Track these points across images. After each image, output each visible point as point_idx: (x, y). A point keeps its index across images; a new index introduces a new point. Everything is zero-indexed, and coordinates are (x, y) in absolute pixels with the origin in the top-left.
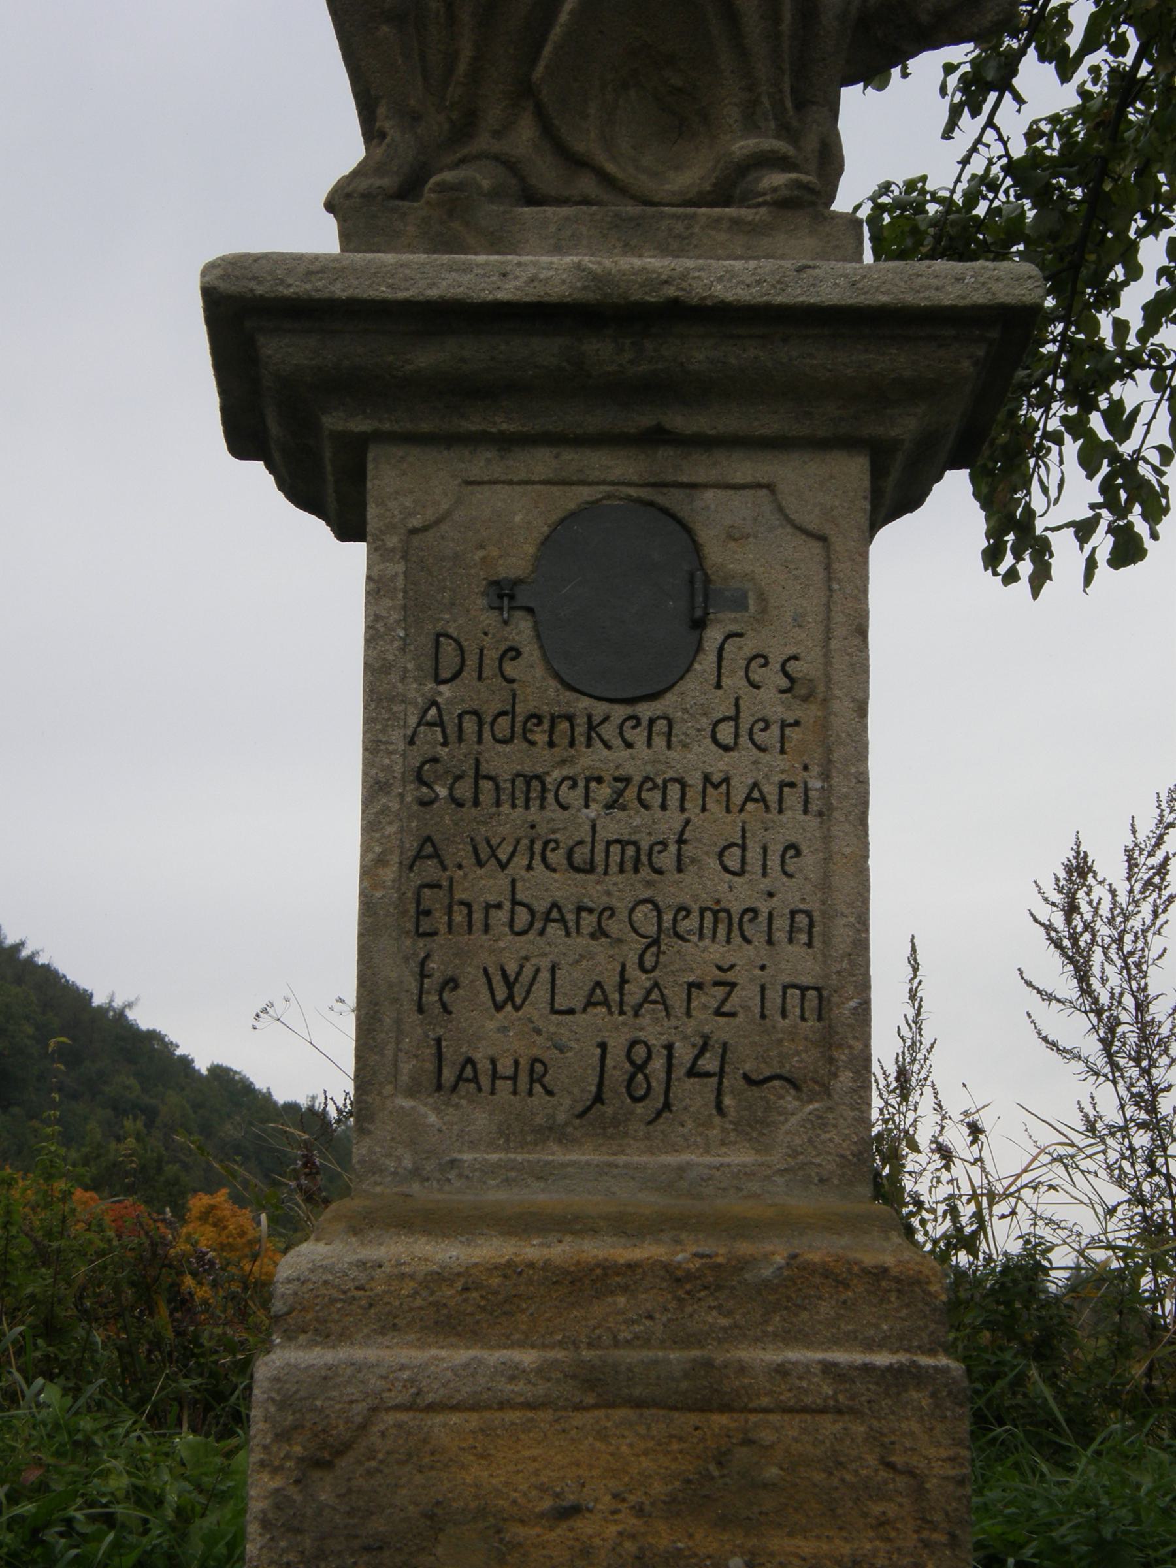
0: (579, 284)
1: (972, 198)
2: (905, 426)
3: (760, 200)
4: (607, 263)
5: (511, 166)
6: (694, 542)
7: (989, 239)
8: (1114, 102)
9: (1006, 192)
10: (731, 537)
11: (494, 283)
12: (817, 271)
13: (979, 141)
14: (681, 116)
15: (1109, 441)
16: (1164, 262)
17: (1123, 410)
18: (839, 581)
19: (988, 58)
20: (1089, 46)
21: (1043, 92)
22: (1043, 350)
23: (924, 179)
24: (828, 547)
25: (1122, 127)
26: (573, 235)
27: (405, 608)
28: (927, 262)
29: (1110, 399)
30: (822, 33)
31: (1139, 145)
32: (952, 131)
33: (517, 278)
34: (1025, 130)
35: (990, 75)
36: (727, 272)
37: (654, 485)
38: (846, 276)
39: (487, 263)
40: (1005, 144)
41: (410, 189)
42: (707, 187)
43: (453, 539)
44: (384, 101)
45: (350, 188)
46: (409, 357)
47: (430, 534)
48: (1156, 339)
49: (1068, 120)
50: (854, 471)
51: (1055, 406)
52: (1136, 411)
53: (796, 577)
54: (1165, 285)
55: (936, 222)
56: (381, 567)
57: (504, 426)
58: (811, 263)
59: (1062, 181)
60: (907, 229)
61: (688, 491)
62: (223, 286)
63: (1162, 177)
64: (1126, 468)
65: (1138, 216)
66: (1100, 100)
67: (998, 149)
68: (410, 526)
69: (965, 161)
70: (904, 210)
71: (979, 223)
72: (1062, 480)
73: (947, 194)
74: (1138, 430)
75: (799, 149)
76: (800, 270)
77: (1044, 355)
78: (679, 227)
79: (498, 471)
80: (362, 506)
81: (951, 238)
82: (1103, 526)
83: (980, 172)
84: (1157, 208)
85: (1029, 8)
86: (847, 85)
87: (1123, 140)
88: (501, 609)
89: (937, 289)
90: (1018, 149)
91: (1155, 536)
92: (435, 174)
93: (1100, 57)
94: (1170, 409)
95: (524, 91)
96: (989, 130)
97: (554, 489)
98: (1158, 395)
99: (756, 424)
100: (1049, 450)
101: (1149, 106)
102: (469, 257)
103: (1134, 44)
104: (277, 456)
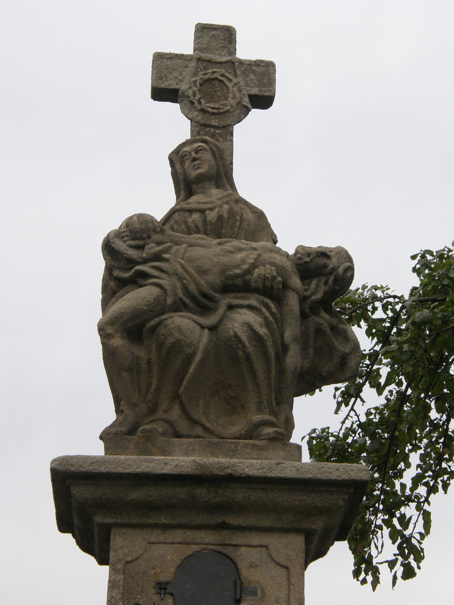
0: (194, 468)
1: (346, 436)
2: (318, 524)
3: (263, 437)
4: (205, 460)
5: (170, 423)
6: (237, 568)
7: (353, 451)
8: (398, 403)
9: (359, 434)
10: (251, 566)
11: (162, 467)
12: (284, 464)
13: (348, 415)
14: (234, 406)
15: (400, 530)
16: (419, 462)
17: (406, 517)
18: (293, 585)
19: (351, 386)
20: (388, 383)
21: (371, 399)
22: (375, 493)
23: (328, 428)
24: (289, 571)
25: (401, 412)
26: (192, 449)
27: (123, 593)
28: (325, 463)
29: (400, 513)
30: (286, 378)
31: (408, 419)
32: (338, 411)
33: (171, 465)
34: (365, 412)
35: (352, 391)
36: (250, 464)
37: (221, 545)
38: (295, 467)
39: (159, 459)
40: (358, 417)
41: (132, 431)
42: (243, 432)
43: (143, 566)
44: (123, 400)
45: (109, 431)
46: (128, 494)
47: (134, 563)
48: (417, 491)
49: (381, 409)
50: (298, 541)
51: (379, 515)
52: (410, 518)
53: (276, 583)
54: (419, 471)
55: (332, 444)
56: (115, 576)
57: (164, 521)
58: (282, 462)
59: (380, 431)
60: (322, 446)
61: (234, 548)
62: (59, 468)
63: (417, 431)
64: (407, 540)
65: (409, 445)
66: (394, 401)
67: (355, 418)
68: (126, 560)
69: (343, 422)
70: (321, 439)
71: (349, 445)
72: (383, 544)
73: (337, 434)
74: (411, 526)
75: (277, 419)
76: (278, 464)
77: (375, 495)
78: (233, 447)
79: (161, 539)
80: (108, 551)
81: (338, 450)
82: (399, 563)
83: (349, 426)
84: (416, 442)
85: (366, 369)
86: (296, 397)
87: (402, 417)
88: (161, 594)
89: (329, 473)
90: (363, 419)
91: (419, 568)
92: (141, 426)
93: (393, 387)
94: (423, 518)
95: (176, 396)
96: (352, 412)
97: (183, 546)
98: (418, 513)
99: (261, 522)
100: (377, 532)
101: (412, 405)
102: (153, 457)
103: (405, 384)
104: (77, 532)
